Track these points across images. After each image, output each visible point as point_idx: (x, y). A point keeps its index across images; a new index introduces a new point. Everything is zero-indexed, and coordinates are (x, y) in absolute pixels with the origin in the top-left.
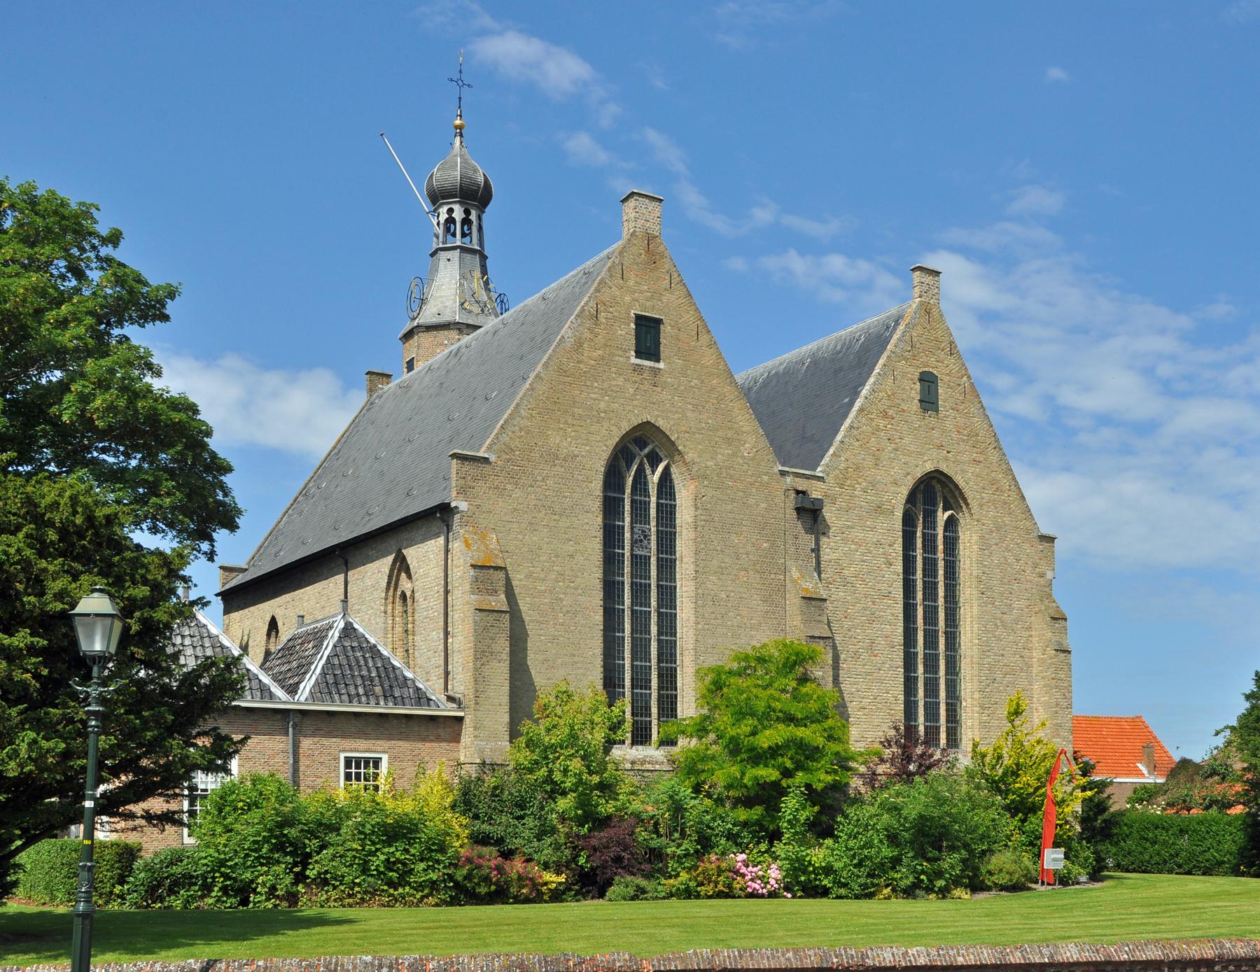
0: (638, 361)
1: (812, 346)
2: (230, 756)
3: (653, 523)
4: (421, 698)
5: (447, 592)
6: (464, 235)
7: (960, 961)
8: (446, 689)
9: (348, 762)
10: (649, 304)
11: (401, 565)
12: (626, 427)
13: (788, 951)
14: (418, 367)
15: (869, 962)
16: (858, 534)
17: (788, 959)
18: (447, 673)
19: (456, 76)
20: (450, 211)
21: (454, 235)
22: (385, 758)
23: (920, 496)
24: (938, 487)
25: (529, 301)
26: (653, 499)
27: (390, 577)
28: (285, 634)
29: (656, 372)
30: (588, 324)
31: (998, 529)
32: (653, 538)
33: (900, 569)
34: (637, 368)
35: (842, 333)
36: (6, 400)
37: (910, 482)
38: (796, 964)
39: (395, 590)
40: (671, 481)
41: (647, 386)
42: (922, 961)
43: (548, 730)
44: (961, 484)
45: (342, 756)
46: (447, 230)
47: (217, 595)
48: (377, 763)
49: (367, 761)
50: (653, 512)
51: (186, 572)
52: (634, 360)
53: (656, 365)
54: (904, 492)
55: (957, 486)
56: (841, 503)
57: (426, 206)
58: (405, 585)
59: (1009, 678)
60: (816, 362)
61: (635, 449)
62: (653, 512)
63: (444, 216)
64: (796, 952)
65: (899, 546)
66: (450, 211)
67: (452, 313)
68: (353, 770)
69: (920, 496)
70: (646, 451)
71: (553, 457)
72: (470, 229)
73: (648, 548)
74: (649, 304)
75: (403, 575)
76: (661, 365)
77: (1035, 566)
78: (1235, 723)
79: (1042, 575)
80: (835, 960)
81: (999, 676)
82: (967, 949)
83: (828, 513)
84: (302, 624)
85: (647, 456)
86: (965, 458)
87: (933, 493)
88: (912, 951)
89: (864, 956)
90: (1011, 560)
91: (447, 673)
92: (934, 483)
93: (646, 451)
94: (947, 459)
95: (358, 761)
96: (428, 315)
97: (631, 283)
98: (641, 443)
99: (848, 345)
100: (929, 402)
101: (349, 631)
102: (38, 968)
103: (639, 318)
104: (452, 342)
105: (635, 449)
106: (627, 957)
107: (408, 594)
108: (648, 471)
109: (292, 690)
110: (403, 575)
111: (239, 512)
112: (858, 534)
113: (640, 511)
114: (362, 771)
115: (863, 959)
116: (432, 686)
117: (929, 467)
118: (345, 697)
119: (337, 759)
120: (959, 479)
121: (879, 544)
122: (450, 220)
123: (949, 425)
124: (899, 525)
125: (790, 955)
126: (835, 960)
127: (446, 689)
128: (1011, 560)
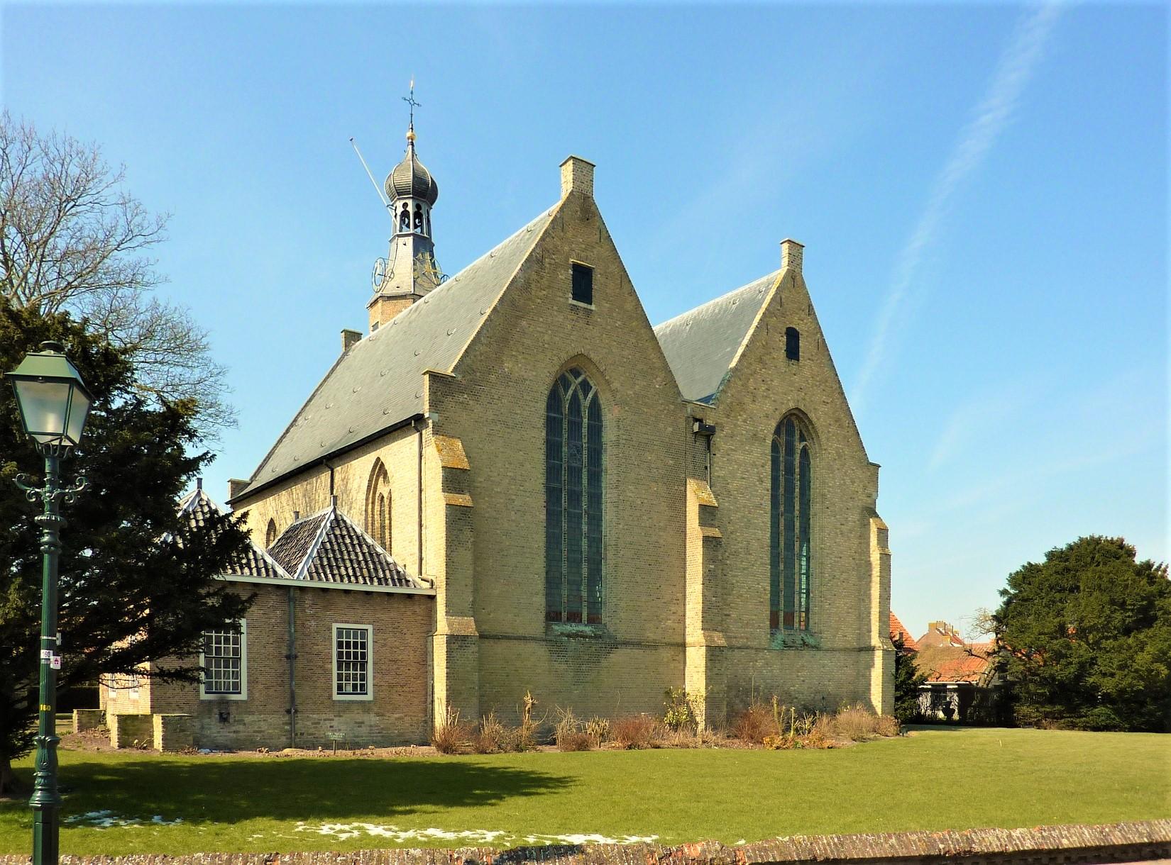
0: (575, 302)
1: (694, 311)
2: (241, 613)
3: (585, 440)
4: (402, 579)
5: (421, 491)
6: (416, 226)
7: (1065, 843)
8: (421, 573)
9: (340, 631)
10: (583, 254)
11: (379, 470)
12: (564, 356)
13: (890, 837)
14: (381, 328)
15: (977, 848)
16: (739, 456)
17: (892, 846)
18: (421, 559)
19: (408, 96)
20: (405, 205)
21: (408, 226)
22: (370, 628)
23: (783, 429)
24: (796, 422)
25: (477, 262)
26: (586, 420)
27: (370, 481)
28: (282, 529)
30: (536, 267)
31: (840, 456)
32: (585, 452)
33: (769, 485)
34: (574, 308)
35: (719, 300)
37: (778, 417)
38: (902, 853)
39: (374, 493)
40: (599, 406)
41: (581, 324)
42: (1029, 845)
46: (402, 221)
50: (585, 431)
51: (194, 424)
52: (571, 301)
53: (589, 307)
54: (774, 424)
55: (810, 422)
56: (727, 431)
57: (386, 200)
58: (382, 489)
59: (844, 576)
60: (697, 323)
61: (571, 378)
62: (585, 431)
63: (400, 210)
64: (898, 837)
65: (768, 467)
66: (405, 205)
67: (407, 287)
69: (783, 429)
70: (580, 379)
71: (507, 379)
72: (421, 221)
73: (581, 460)
74: (583, 254)
75: (381, 479)
76: (593, 307)
77: (865, 488)
80: (941, 846)
81: (837, 574)
82: (1068, 830)
83: (718, 439)
84: (297, 517)
85: (580, 384)
87: (793, 427)
88: (1016, 833)
89: (970, 841)
90: (848, 482)
91: (421, 559)
92: (793, 418)
93: (580, 379)
96: (390, 289)
97: (569, 235)
98: (576, 373)
99: (724, 310)
100: (793, 352)
101: (338, 522)
102: (10, 860)
103: (576, 267)
104: (409, 308)
105: (571, 378)
106: (718, 847)
107: (386, 495)
108: (581, 397)
109: (290, 569)
110: (381, 479)
112: (739, 456)
113: (575, 427)
115: (970, 845)
116: (412, 572)
117: (792, 405)
118: (338, 578)
119: (330, 629)
120: (812, 415)
121: (754, 465)
122: (405, 214)
123: (806, 372)
124: (768, 450)
125: (893, 841)
126: (941, 846)
127: (421, 573)
128: (848, 482)
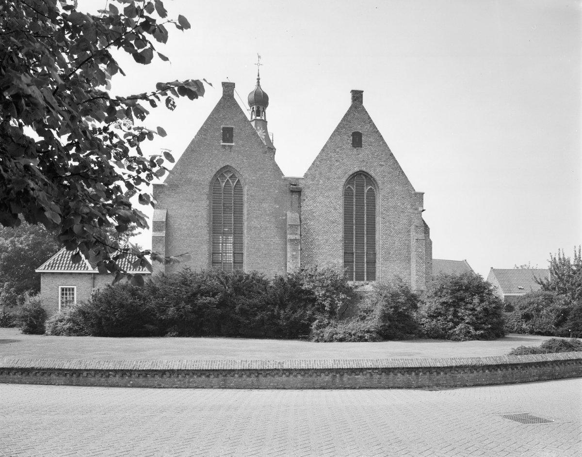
0: (224, 144)
9: (63, 289)
29: (231, 147)
34: (224, 146)
36: (4, 21)
43: (318, 290)
44: (373, 175)
45: (60, 287)
47: (153, 185)
48: (73, 289)
49: (69, 289)
53: (231, 144)
68: (65, 292)
78: (247, 270)
79: (416, 209)
86: (375, 164)
94: (366, 166)
95: (66, 289)
111: (203, 96)
114: (65, 292)
